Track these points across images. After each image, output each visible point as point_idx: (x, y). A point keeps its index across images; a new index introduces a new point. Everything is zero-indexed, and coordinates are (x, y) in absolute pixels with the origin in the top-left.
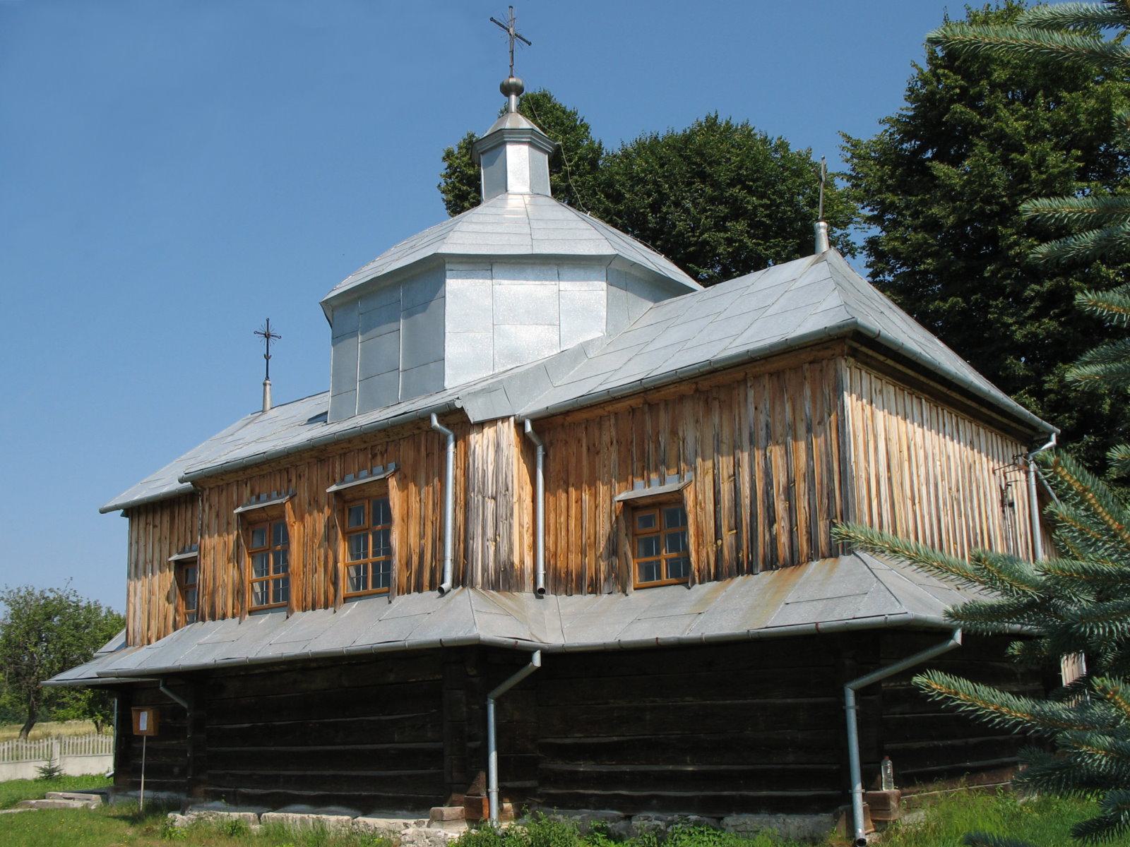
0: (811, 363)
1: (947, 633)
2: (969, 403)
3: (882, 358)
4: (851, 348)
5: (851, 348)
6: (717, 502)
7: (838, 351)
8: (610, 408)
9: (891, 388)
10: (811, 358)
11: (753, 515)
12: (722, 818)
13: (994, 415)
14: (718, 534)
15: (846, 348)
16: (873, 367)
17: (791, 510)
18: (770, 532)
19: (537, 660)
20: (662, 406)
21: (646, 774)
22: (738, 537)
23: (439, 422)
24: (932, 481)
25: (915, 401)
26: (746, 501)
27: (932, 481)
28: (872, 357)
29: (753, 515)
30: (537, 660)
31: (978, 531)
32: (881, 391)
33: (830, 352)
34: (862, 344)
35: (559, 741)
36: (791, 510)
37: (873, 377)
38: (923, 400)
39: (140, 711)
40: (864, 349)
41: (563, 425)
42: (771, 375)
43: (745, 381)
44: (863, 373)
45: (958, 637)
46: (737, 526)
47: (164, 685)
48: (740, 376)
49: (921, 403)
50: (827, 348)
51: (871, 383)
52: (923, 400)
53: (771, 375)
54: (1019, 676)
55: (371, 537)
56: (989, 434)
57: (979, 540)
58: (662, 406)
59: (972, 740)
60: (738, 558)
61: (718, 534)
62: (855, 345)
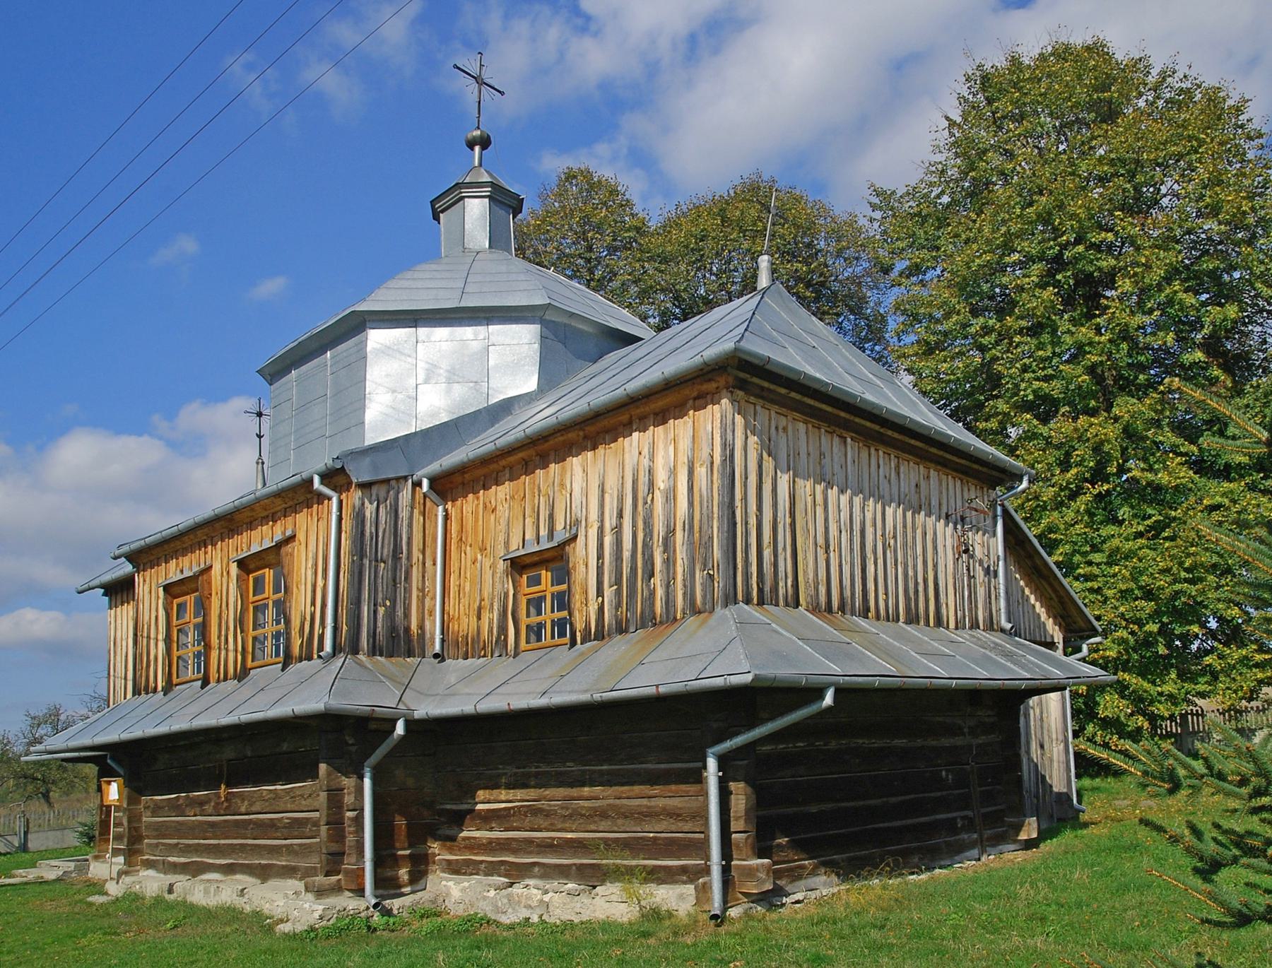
0: (695, 399)
1: (819, 692)
2: (913, 442)
3: (783, 391)
4: (737, 378)
5: (737, 378)
6: (600, 556)
7: (722, 382)
8: (503, 463)
9: (802, 427)
10: (695, 394)
11: (634, 569)
12: (594, 887)
13: (948, 456)
14: (600, 592)
15: (731, 380)
16: (773, 402)
17: (669, 562)
18: (648, 586)
19: (400, 729)
20: (552, 453)
21: (529, 841)
22: (618, 593)
23: (322, 483)
24: (857, 527)
25: (836, 440)
26: (626, 554)
27: (857, 527)
28: (768, 390)
29: (634, 569)
30: (400, 729)
31: (920, 580)
32: (785, 429)
33: (714, 385)
34: (753, 375)
35: (454, 807)
36: (669, 562)
37: (773, 413)
38: (849, 440)
39: (109, 783)
40: (755, 380)
41: (463, 484)
42: (656, 414)
43: (630, 423)
44: (758, 408)
45: (828, 700)
46: (618, 582)
47: (113, 758)
48: (625, 418)
49: (845, 442)
50: (710, 380)
51: (770, 420)
52: (849, 440)
53: (656, 414)
54: (966, 730)
55: (658, 609)
56: (944, 477)
57: (921, 588)
58: (552, 453)
59: (893, 800)
60: (616, 616)
61: (600, 592)
62: (742, 375)
